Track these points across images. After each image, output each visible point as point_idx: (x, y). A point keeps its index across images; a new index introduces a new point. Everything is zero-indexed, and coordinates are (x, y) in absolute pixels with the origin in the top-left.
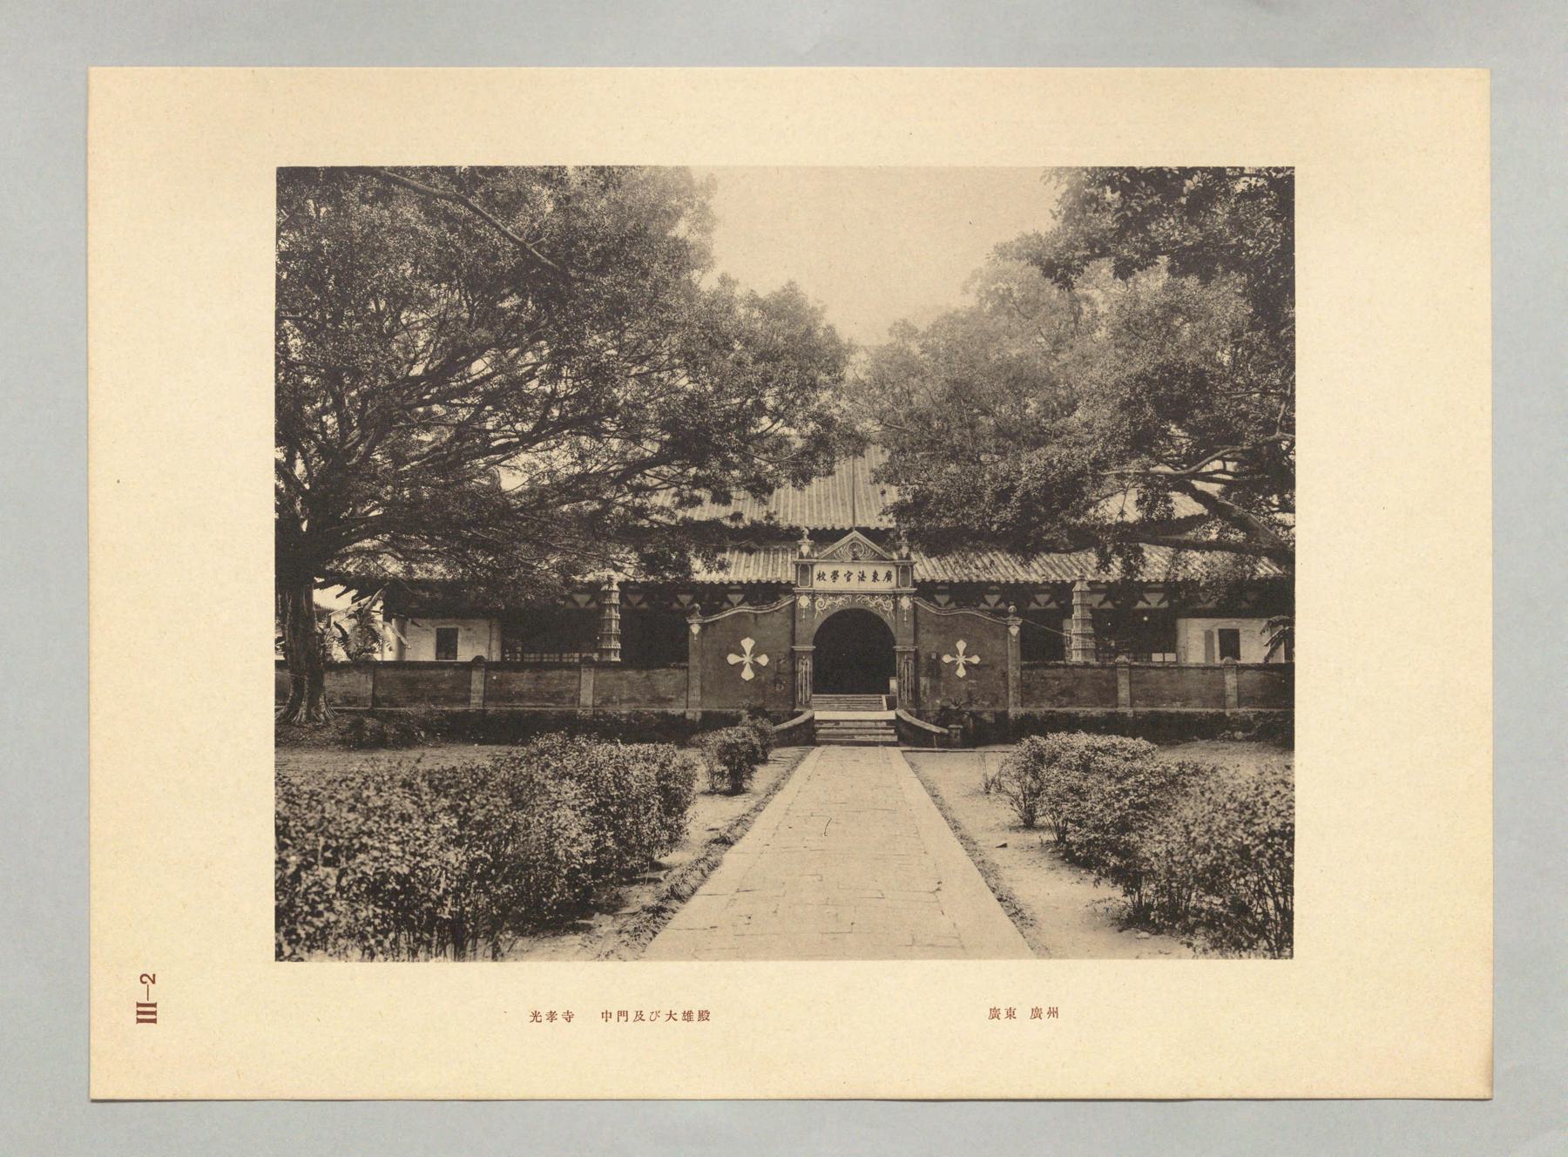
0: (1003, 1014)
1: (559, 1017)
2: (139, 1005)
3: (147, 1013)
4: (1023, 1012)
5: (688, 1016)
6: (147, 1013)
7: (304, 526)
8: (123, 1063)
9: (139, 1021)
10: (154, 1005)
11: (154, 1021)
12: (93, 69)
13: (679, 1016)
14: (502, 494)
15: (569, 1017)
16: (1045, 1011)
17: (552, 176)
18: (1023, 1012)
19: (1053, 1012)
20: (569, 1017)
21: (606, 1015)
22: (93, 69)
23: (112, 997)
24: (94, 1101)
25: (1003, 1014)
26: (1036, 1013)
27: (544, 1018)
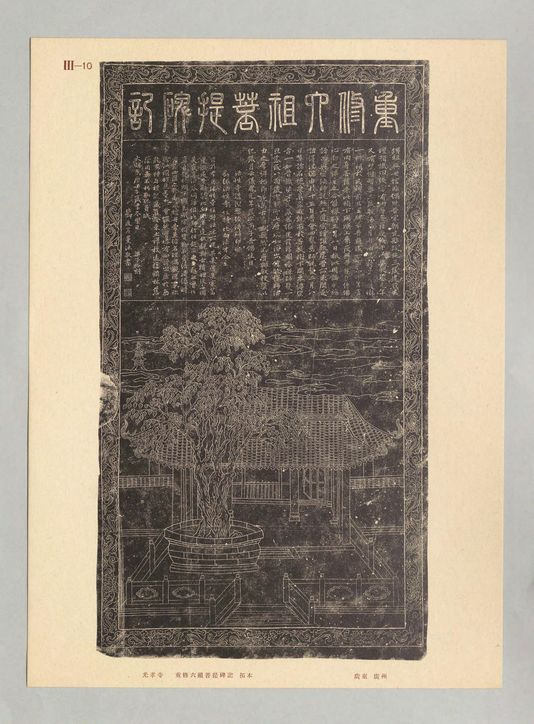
0: (361, 677)
1: (156, 675)
2: (72, 62)
3: (69, 65)
5: (208, 675)
6: (69, 65)
9: (65, 62)
10: (72, 69)
11: (65, 69)
12: (505, 42)
13: (197, 675)
15: (160, 675)
19: (384, 676)
20: (160, 675)
21: (249, 676)
24: (30, 39)
25: (361, 677)
27: (149, 675)
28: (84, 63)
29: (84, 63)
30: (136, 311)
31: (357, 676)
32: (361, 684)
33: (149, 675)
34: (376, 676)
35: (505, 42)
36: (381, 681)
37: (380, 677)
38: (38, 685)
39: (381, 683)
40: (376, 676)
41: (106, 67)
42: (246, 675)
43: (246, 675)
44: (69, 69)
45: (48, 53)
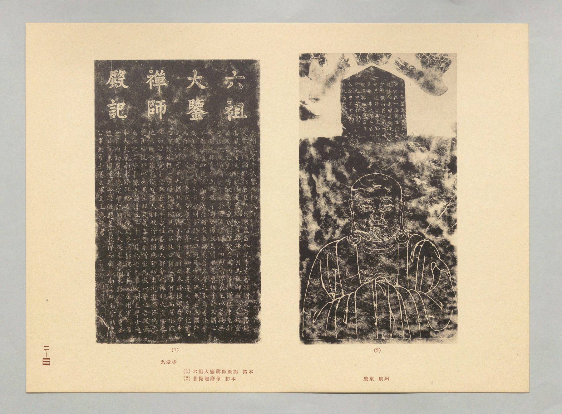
0: (369, 379)
1: (171, 362)
2: (44, 359)
3: (46, 362)
4: (376, 379)
5: (169, 362)
6: (46, 362)
7: (189, 335)
8: (38, 379)
10: (49, 359)
12: (28, 25)
13: (198, 372)
14: (308, 245)
15: (175, 362)
16: (384, 378)
17: (428, 54)
18: (376, 379)
20: (175, 362)
21: (251, 372)
22: (28, 25)
23: (34, 356)
25: (369, 379)
26: (381, 379)
27: (166, 363)
30: (205, 246)
33: (166, 363)
37: (384, 380)
41: (118, 79)
42: (248, 372)
43: (248, 372)
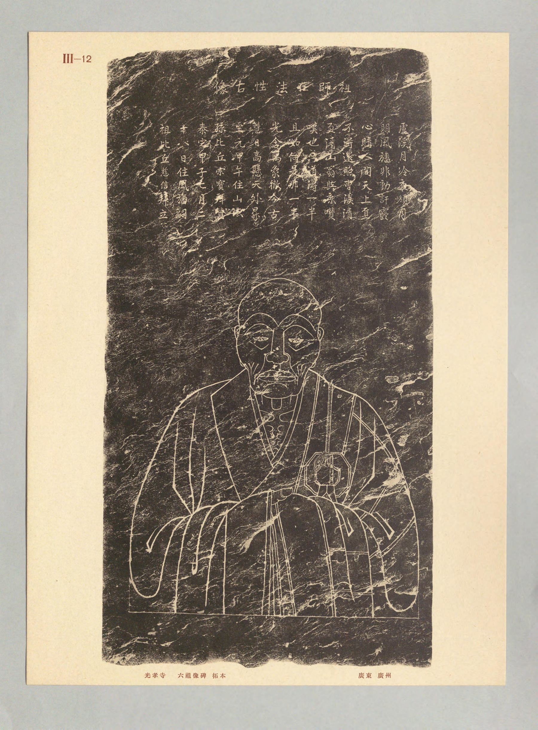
0: (365, 676)
1: (159, 676)
2: (72, 55)
3: (68, 58)
6: (68, 58)
9: (64, 55)
10: (72, 62)
12: (508, 34)
13: (184, 676)
20: (163, 676)
25: (365, 676)
27: (152, 676)
28: (84, 57)
29: (84, 57)
31: (388, 675)
32: (366, 682)
34: (369, 676)
35: (508, 34)
36: (159, 679)
37: (384, 677)
38: (503, 34)
39: (385, 682)
40: (215, 676)
42: (219, 676)
43: (219, 676)
44: (68, 62)
45: (46, 47)
